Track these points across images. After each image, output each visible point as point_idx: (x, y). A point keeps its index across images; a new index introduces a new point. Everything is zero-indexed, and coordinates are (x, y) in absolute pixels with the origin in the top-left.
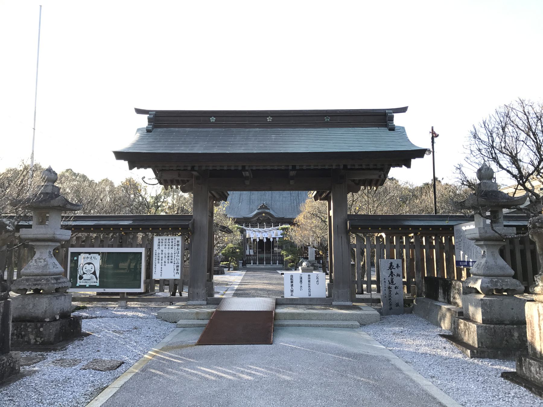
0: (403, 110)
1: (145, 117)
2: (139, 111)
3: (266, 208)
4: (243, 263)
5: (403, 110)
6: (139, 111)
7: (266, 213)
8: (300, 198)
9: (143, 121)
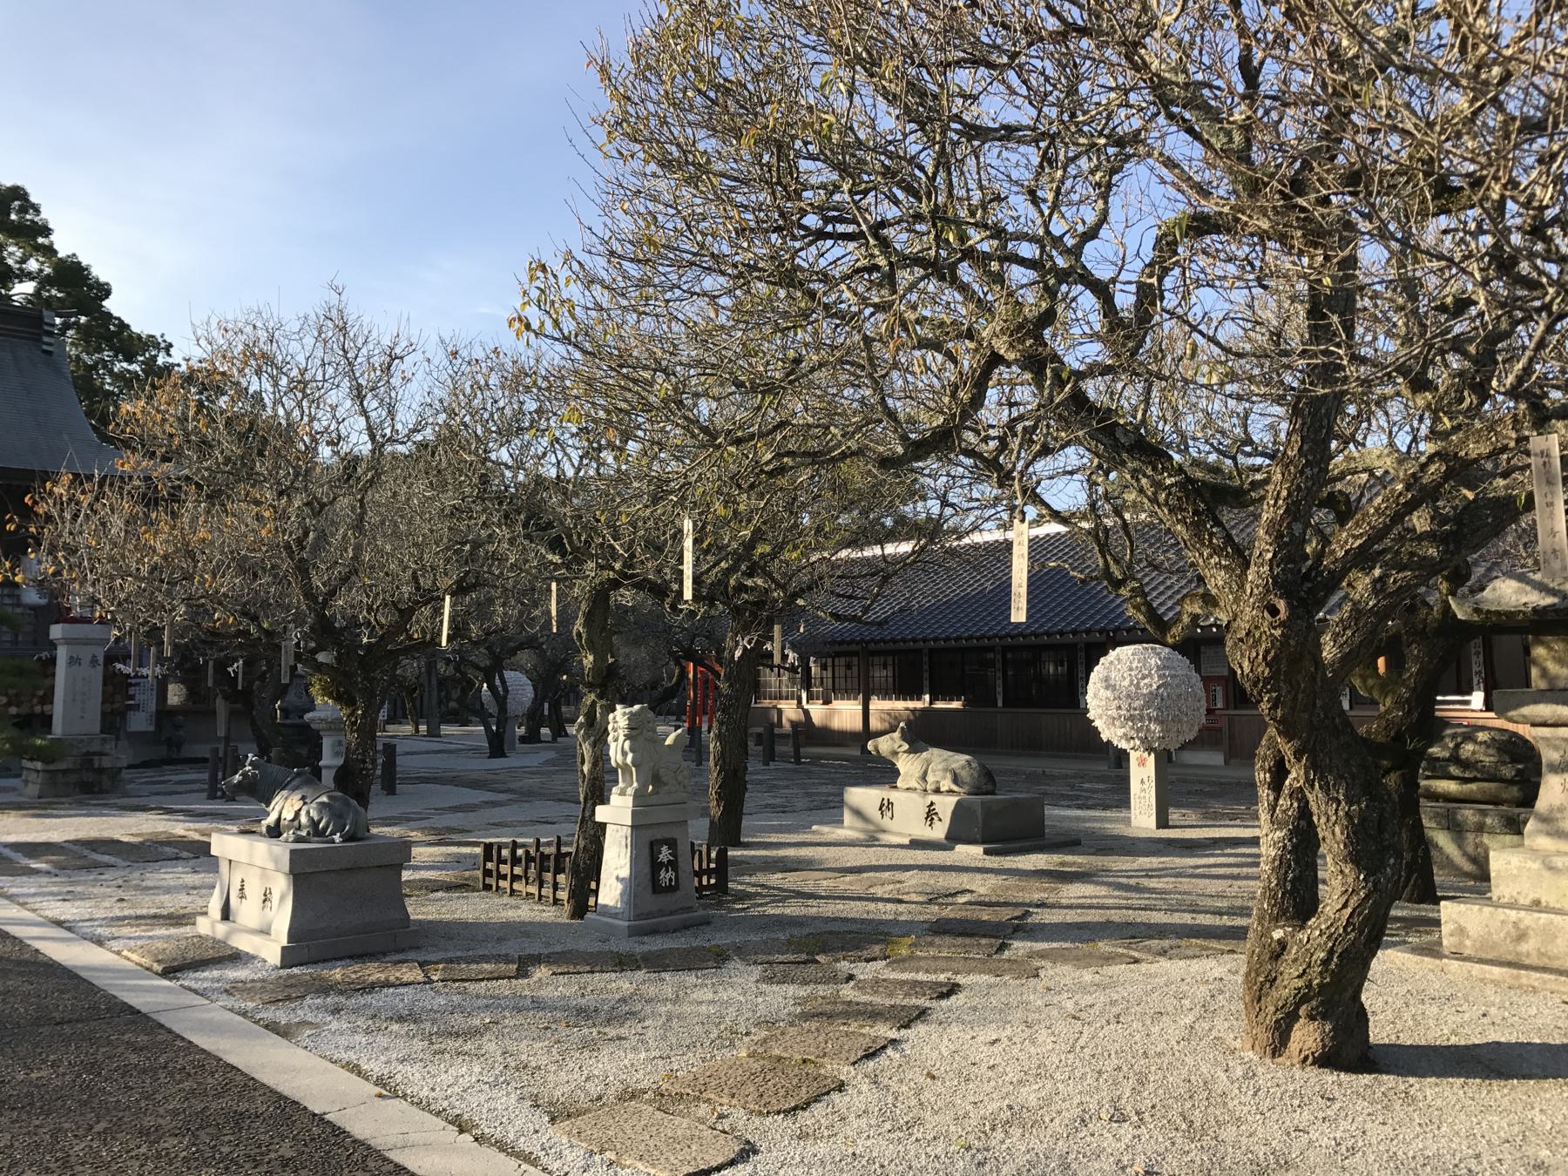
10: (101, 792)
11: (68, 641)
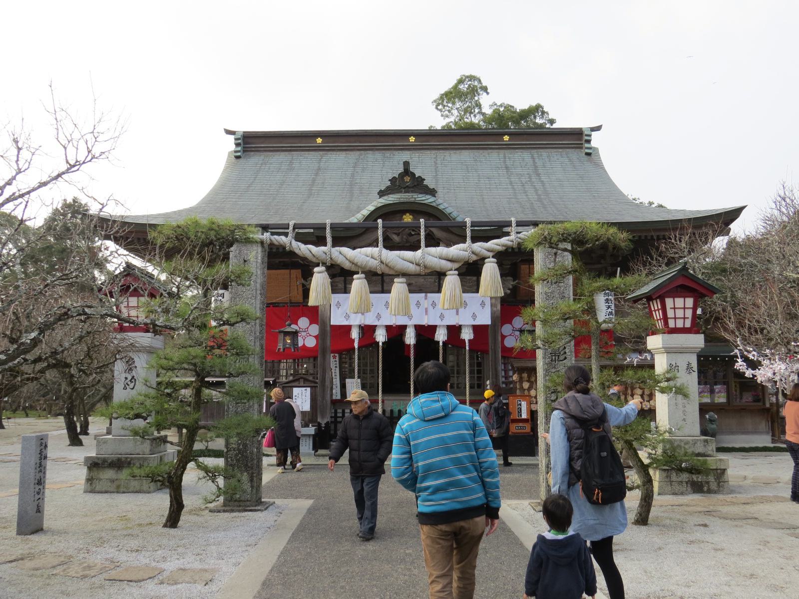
0: (598, 128)
1: (232, 137)
2: (229, 132)
3: (418, 184)
4: (315, 437)
5: (598, 128)
6: (229, 132)
7: (419, 210)
8: (543, 178)
9: (230, 144)
10: (709, 491)
11: (669, 351)
